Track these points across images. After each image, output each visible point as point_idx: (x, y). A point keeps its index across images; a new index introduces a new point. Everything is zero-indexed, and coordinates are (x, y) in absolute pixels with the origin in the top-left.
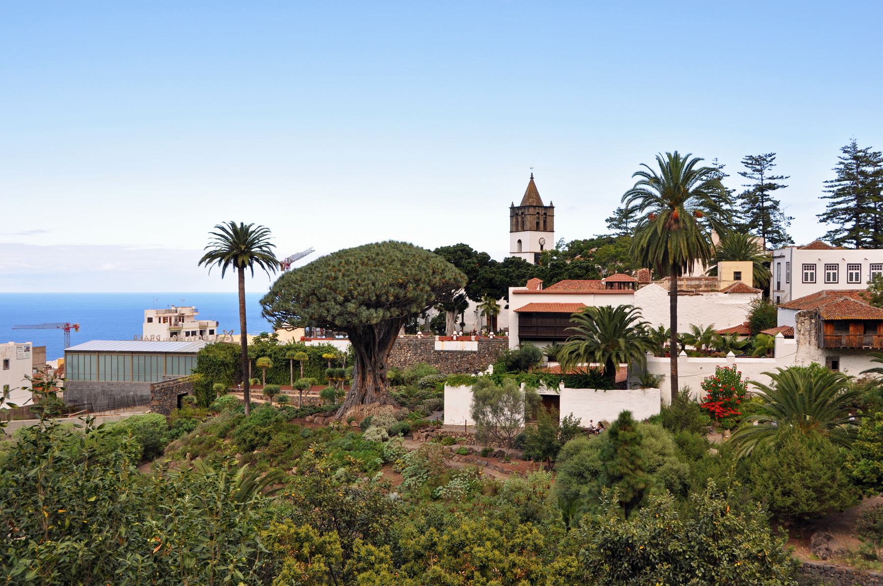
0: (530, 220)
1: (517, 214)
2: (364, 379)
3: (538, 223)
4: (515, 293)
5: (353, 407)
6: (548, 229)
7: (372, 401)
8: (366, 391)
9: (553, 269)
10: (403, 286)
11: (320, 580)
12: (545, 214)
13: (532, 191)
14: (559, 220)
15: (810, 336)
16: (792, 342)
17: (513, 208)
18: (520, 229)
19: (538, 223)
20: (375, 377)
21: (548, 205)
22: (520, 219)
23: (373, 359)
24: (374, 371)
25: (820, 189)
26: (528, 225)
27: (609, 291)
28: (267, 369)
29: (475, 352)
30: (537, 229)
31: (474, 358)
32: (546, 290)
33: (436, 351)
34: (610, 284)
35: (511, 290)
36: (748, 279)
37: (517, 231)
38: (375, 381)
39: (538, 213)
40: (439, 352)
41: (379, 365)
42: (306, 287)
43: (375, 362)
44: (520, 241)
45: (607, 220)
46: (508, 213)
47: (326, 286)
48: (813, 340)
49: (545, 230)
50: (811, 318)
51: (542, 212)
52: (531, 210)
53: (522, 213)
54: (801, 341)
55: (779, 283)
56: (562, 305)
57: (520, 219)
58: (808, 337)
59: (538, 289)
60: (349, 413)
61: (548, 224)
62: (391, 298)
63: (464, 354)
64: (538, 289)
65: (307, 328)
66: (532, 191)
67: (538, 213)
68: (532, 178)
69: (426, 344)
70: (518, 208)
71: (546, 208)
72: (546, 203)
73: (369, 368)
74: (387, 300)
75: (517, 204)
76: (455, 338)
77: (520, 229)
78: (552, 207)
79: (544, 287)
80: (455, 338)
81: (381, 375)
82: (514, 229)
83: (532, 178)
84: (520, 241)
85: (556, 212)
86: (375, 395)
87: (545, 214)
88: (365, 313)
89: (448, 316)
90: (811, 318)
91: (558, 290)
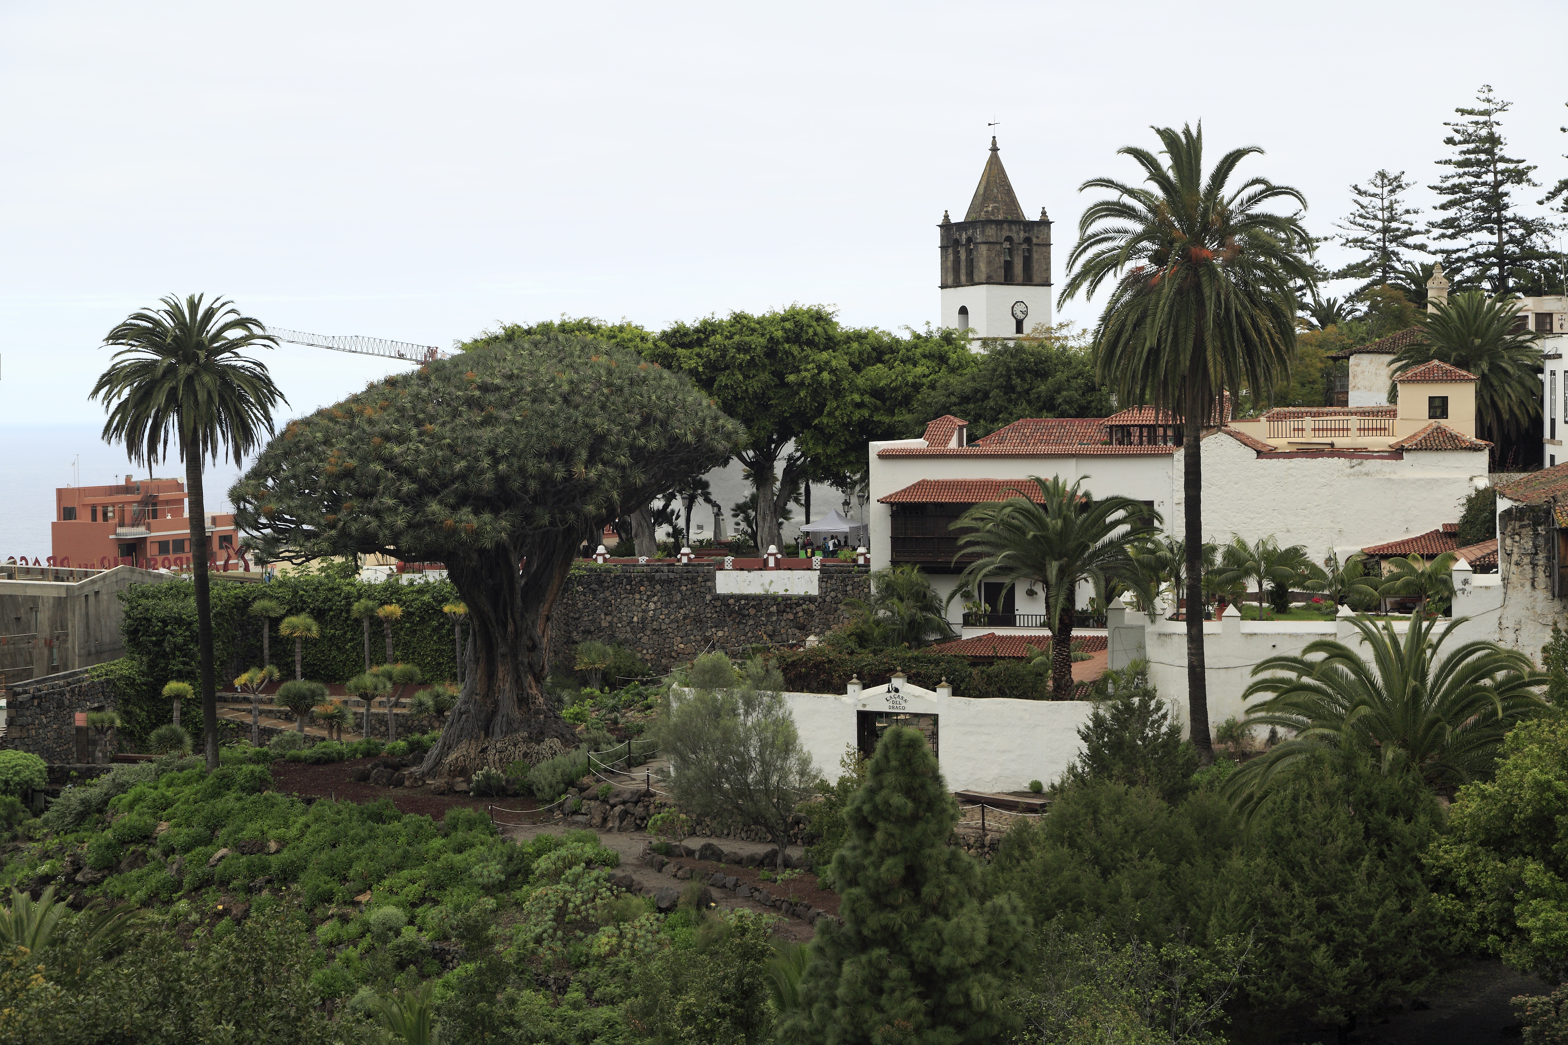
1: (957, 242)
2: (491, 676)
3: (1008, 266)
4: (884, 456)
5: (464, 745)
6: (1036, 279)
7: (510, 728)
8: (496, 703)
9: (1018, 388)
10: (564, 455)
11: (1559, 860)
12: (1028, 240)
13: (995, 183)
15: (1534, 565)
16: (1493, 579)
17: (947, 227)
18: (963, 278)
20: (516, 670)
21: (1035, 217)
22: (963, 256)
23: (510, 628)
24: (515, 656)
26: (982, 269)
27: (1115, 448)
28: (307, 641)
29: (809, 599)
30: (1008, 280)
31: (808, 613)
32: (983, 446)
33: (718, 597)
34: (1123, 433)
35: (876, 447)
36: (1462, 417)
37: (957, 284)
38: (518, 682)
39: (1009, 239)
40: (725, 598)
41: (525, 641)
42: (334, 459)
43: (517, 634)
44: (963, 311)
46: (935, 238)
47: (380, 458)
48: (1541, 575)
49: (1028, 281)
50: (1536, 524)
52: (991, 231)
53: (969, 240)
54: (1513, 578)
55: (1553, 421)
57: (963, 256)
58: (1528, 568)
59: (953, 444)
60: (452, 757)
61: (1035, 266)
62: (533, 485)
63: (787, 604)
64: (953, 444)
65: (799, 454)
66: (995, 183)
67: (1009, 239)
68: (994, 149)
69: (693, 580)
70: (958, 225)
71: (1030, 225)
72: (1031, 214)
73: (502, 650)
74: (524, 487)
75: (958, 216)
76: (772, 563)
77: (963, 278)
78: (1045, 223)
79: (972, 439)
80: (772, 563)
81: (531, 665)
82: (950, 281)
83: (994, 149)
84: (963, 311)
86: (517, 714)
87: (1028, 240)
88: (467, 518)
90: (1536, 524)
91: (1008, 448)
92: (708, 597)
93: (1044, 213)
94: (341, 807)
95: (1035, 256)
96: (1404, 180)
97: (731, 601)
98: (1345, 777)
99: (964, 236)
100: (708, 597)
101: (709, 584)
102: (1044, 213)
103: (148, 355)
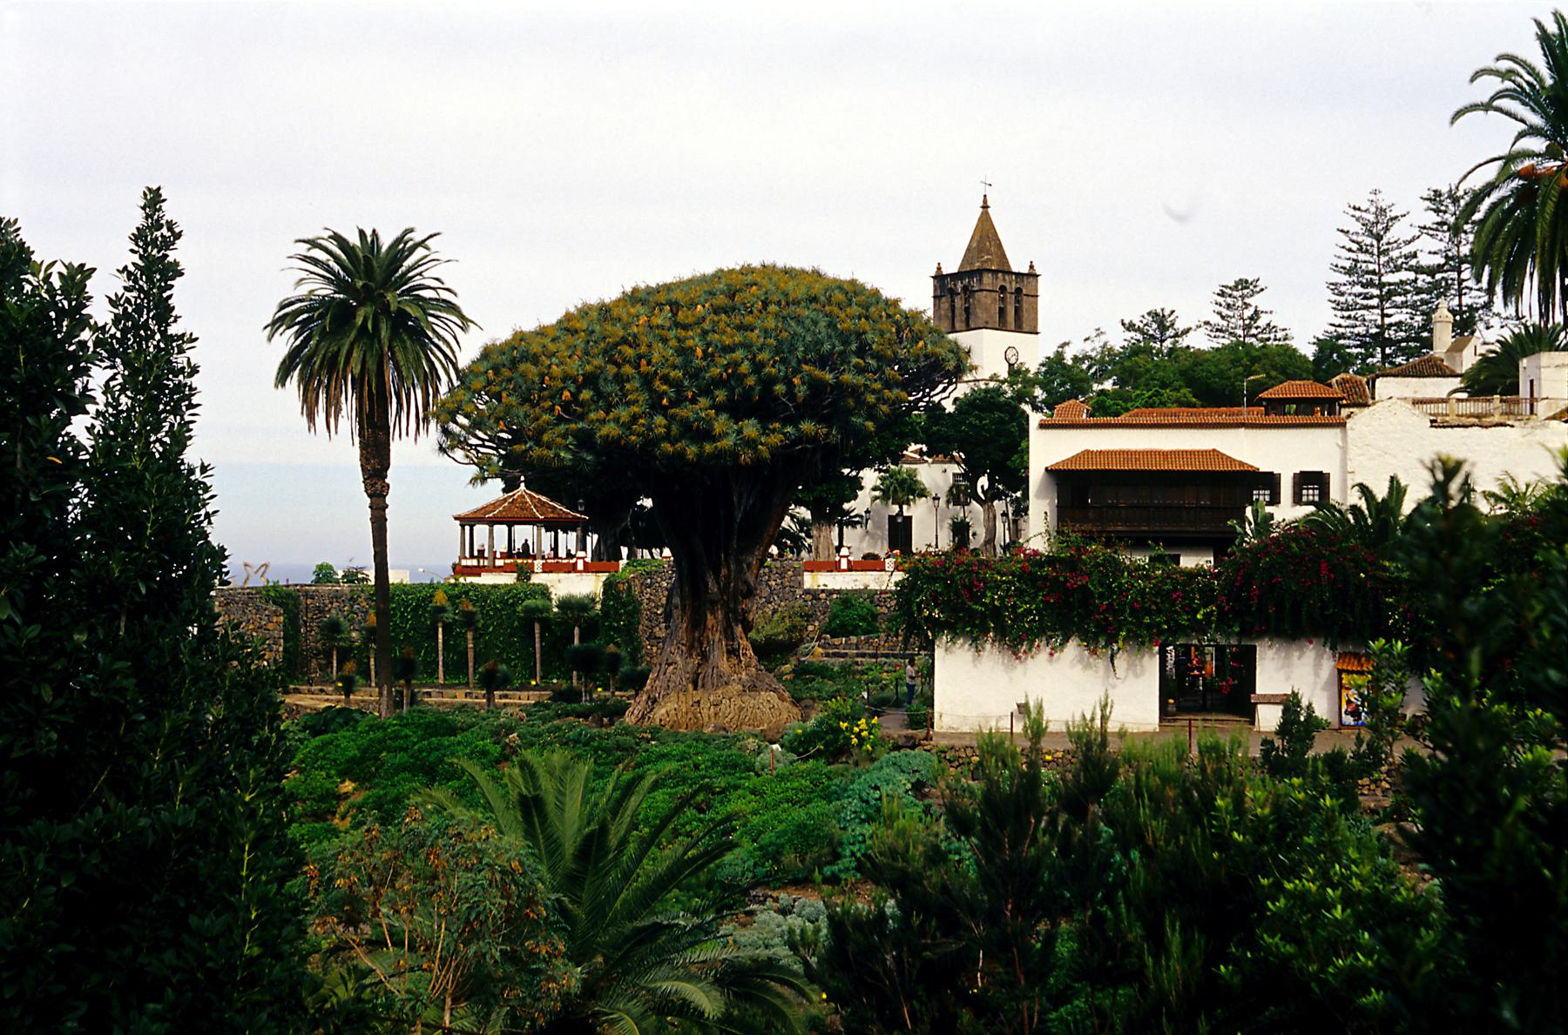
0: (987, 302)
1: (953, 293)
3: (1002, 312)
12: (1019, 291)
13: (985, 237)
14: (1049, 302)
17: (939, 278)
19: (1002, 312)
21: (1025, 270)
22: (959, 302)
25: (877, 285)
26: (980, 314)
30: (1002, 326)
33: (807, 592)
45: (282, 379)
49: (1019, 329)
51: (1012, 286)
53: (965, 288)
56: (1165, 455)
61: (1025, 315)
66: (985, 237)
67: (1003, 289)
68: (985, 207)
72: (1018, 265)
75: (951, 267)
76: (844, 565)
77: (958, 325)
78: (1032, 275)
80: (844, 565)
83: (985, 207)
85: (1043, 286)
87: (1019, 291)
89: (1456, 383)
92: (799, 592)
93: (1031, 267)
94: (848, 852)
95: (1025, 306)
96: (1261, 284)
97: (823, 596)
98: (69, 647)
99: (959, 285)
100: (799, 592)
101: (1426, 509)
102: (1031, 267)
103: (297, 372)
